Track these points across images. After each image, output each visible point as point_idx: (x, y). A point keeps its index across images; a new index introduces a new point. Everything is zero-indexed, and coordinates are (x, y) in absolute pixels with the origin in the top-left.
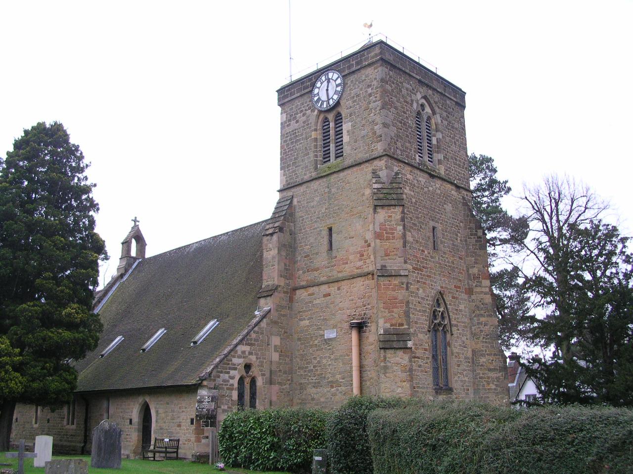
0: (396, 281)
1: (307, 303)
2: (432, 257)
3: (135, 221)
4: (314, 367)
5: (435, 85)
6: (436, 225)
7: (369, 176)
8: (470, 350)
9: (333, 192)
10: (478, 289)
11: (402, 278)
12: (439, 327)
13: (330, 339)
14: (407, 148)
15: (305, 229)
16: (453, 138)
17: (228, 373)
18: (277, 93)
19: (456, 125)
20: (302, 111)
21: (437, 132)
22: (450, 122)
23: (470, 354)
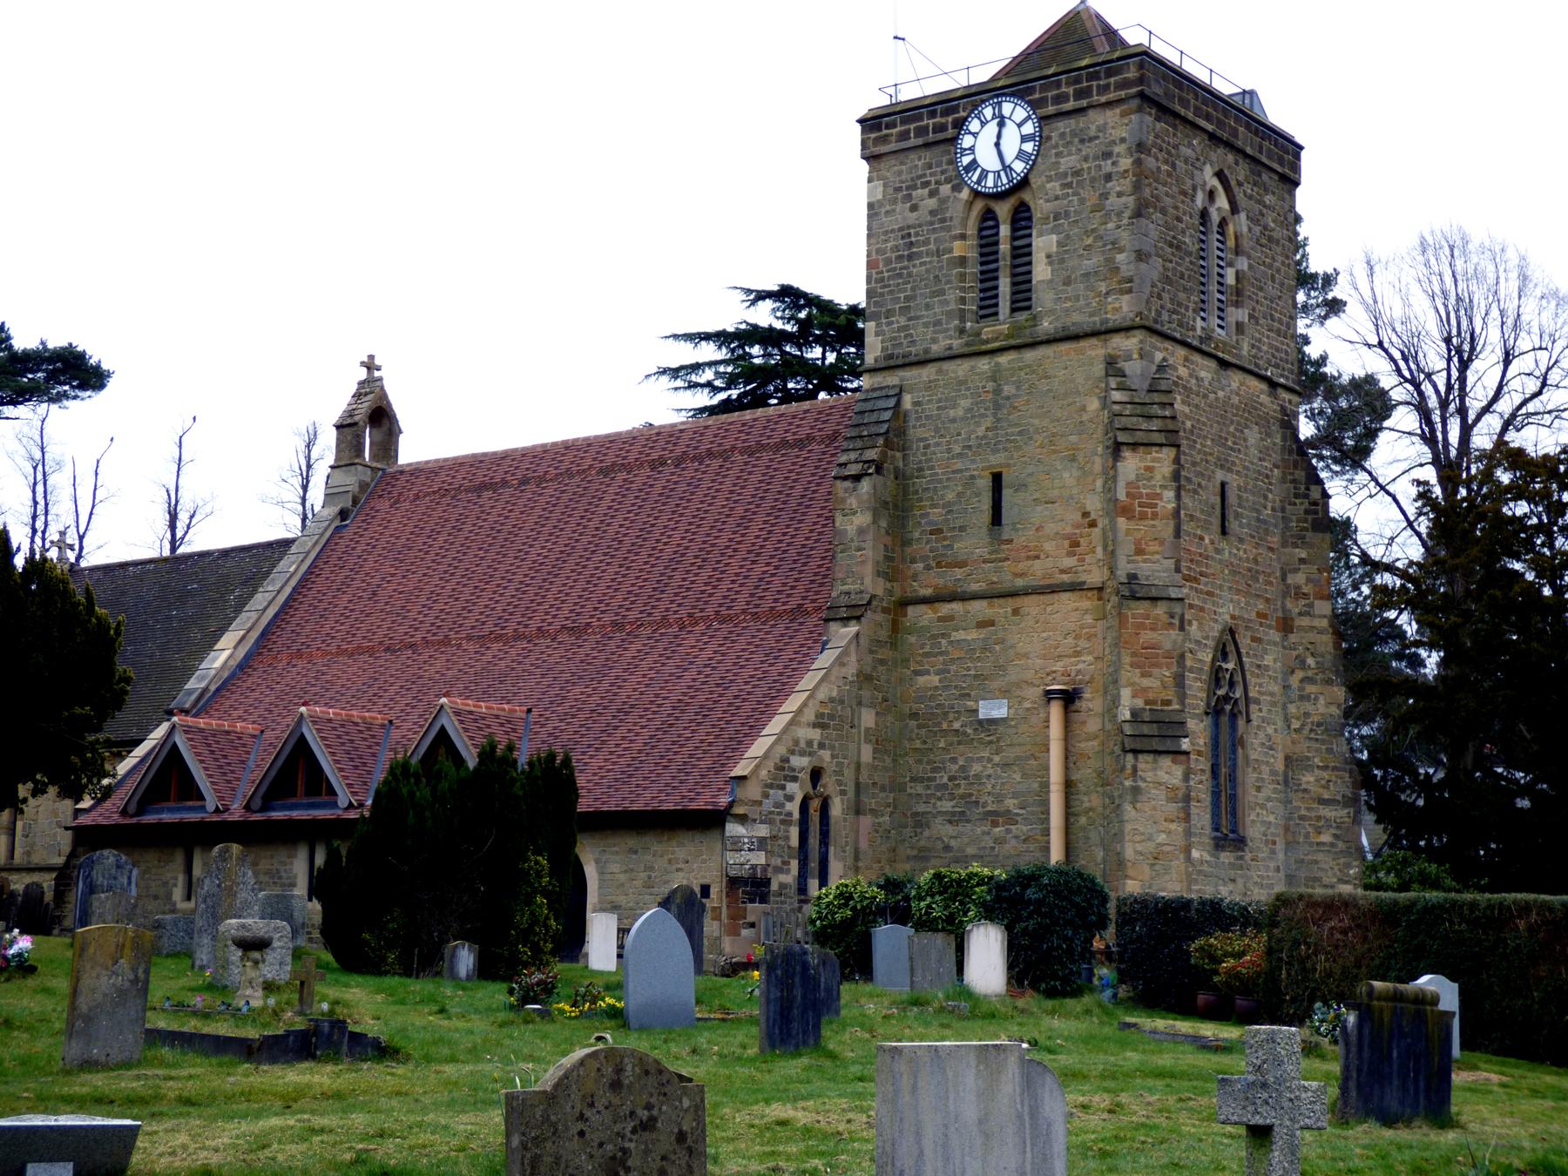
0: (1160, 610)
1: (934, 637)
2: (1218, 551)
3: (370, 365)
4: (951, 779)
5: (1244, 139)
7: (1099, 369)
8: (1281, 756)
9: (1005, 393)
10: (1305, 622)
11: (1173, 604)
12: (1227, 711)
15: (932, 468)
18: (858, 127)
20: (927, 184)
21: (1237, 254)
22: (1265, 228)
23: (1280, 766)
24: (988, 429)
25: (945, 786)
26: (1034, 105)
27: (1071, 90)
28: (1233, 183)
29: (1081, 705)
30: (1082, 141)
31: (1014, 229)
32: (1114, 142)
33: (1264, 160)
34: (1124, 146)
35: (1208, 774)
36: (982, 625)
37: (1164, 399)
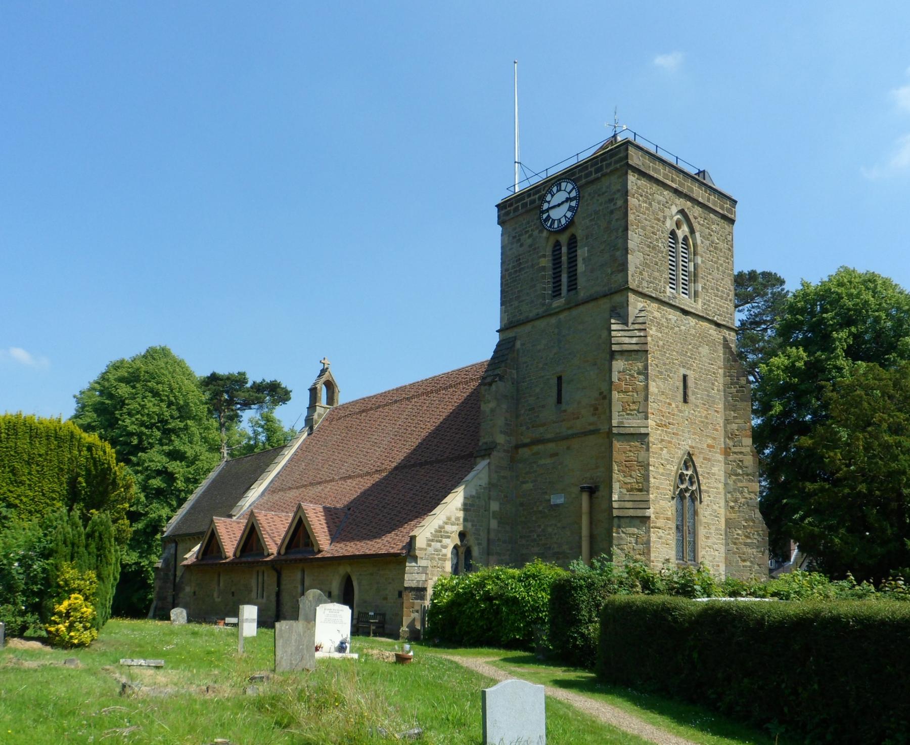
2: (680, 411)
4: (538, 536)
6: (688, 373)
8: (723, 521)
14: (655, 278)
17: (440, 541)
18: (496, 209)
19: (721, 245)
22: (713, 242)
25: (535, 540)
26: (575, 181)
27: (593, 169)
28: (691, 217)
29: (597, 493)
30: (599, 195)
31: (569, 249)
32: (615, 193)
33: (710, 205)
35: (674, 530)
36: (553, 455)
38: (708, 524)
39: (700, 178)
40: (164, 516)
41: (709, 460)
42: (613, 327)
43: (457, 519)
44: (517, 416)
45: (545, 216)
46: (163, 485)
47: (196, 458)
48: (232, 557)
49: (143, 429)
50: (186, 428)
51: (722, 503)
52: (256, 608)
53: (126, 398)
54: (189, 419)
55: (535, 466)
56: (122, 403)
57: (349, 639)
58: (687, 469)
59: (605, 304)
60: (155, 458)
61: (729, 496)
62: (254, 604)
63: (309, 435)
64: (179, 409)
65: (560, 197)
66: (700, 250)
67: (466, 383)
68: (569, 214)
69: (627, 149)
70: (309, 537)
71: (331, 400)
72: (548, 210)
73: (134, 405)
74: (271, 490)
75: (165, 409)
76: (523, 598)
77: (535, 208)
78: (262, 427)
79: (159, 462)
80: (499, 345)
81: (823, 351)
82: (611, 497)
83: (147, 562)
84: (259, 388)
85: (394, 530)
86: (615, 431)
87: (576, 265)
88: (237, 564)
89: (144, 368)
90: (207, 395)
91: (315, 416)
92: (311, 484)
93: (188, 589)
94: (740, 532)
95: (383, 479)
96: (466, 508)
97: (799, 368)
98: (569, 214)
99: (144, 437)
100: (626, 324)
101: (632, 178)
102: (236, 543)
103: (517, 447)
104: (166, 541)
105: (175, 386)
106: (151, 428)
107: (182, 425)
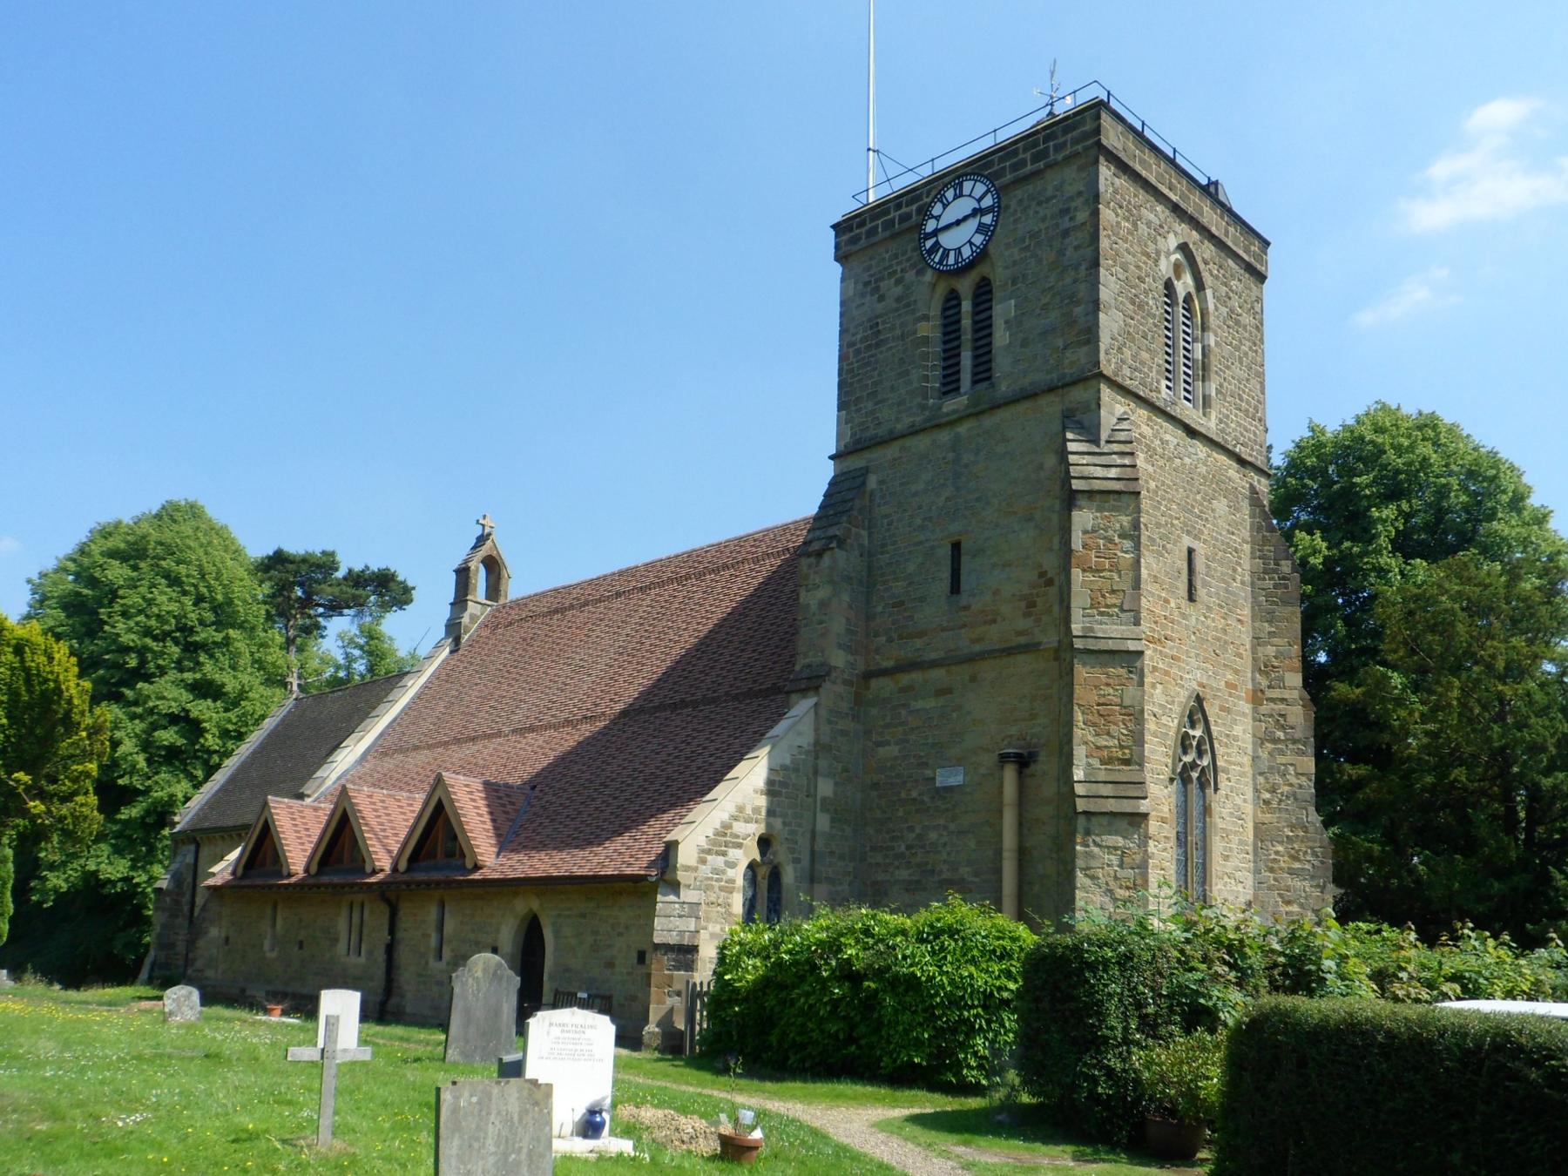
4: (909, 847)
6: (1196, 545)
8: (1250, 825)
13: (950, 789)
14: (1143, 363)
16: (1237, 349)
17: (724, 854)
19: (1246, 319)
20: (895, 272)
22: (1232, 311)
24: (948, 499)
26: (990, 178)
27: (1028, 155)
28: (1199, 259)
29: (1033, 768)
30: (1040, 204)
31: (975, 305)
32: (1071, 199)
33: (1230, 243)
34: (1081, 199)
35: (1173, 842)
36: (942, 692)
37: (1126, 448)
38: (1228, 833)
39: (1210, 190)
40: (180, 796)
41: (1228, 710)
42: (1072, 447)
43: (756, 810)
44: (870, 617)
45: (929, 244)
46: (181, 742)
47: (242, 695)
48: (301, 874)
49: (148, 641)
50: (227, 642)
51: (1250, 794)
52: (358, 995)
53: (121, 587)
54: (233, 627)
55: (904, 712)
56: (113, 595)
57: (608, 1101)
58: (1193, 727)
59: (1051, 406)
60: (168, 693)
61: (1261, 779)
62: (355, 988)
63: (452, 652)
64: (215, 609)
65: (963, 206)
66: (1213, 321)
67: (756, 561)
68: (979, 240)
69: (1098, 117)
70: (455, 838)
71: (494, 591)
72: (936, 233)
73: (133, 599)
74: (380, 750)
75: (190, 608)
76: (931, 979)
77: (909, 229)
78: (361, 648)
79: (175, 700)
80: (833, 483)
81: (1354, 539)
82: (1071, 775)
83: (144, 878)
84: (357, 580)
85: (627, 829)
86: (1078, 644)
87: (990, 335)
88: (311, 887)
89: (154, 535)
90: (267, 588)
91: (465, 620)
92: (457, 741)
93: (214, 932)
94: (1280, 848)
95: (599, 733)
96: (773, 789)
97: (1314, 568)
98: (979, 240)
99: (149, 656)
100: (1096, 442)
101: (1105, 172)
102: (309, 847)
103: (868, 676)
104: (180, 839)
105: (209, 568)
106: (163, 641)
107: (219, 637)
